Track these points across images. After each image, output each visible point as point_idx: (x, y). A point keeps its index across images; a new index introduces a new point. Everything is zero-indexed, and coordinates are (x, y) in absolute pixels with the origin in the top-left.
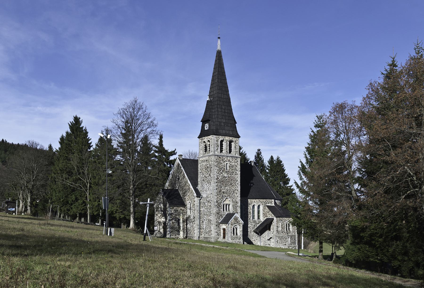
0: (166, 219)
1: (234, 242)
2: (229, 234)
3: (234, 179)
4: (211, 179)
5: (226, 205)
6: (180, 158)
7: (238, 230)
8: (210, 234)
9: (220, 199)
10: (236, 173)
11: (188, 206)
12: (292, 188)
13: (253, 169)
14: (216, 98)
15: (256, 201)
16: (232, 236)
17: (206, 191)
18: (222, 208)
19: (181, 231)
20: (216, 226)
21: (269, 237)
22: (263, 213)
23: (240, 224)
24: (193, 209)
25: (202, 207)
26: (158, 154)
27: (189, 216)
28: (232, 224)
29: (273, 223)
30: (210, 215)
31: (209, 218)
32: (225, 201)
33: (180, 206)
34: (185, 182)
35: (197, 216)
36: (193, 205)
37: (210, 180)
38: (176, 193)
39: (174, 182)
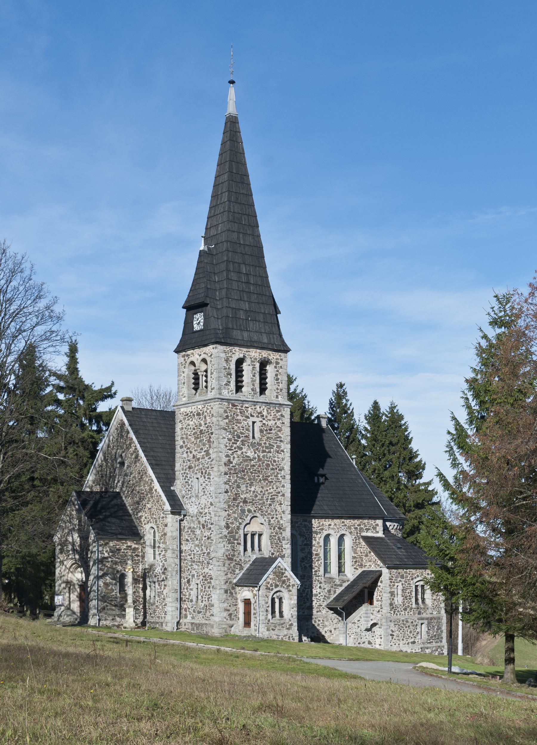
0: (88, 575)
1: (275, 637)
2: (261, 613)
3: (273, 465)
5: (253, 535)
8: (208, 614)
9: (236, 519)
11: (148, 538)
15: (333, 524)
16: (269, 621)
17: (197, 496)
19: (129, 607)
20: (226, 592)
21: (368, 621)
23: (291, 588)
24: (161, 545)
25: (187, 540)
27: (152, 566)
28: (268, 588)
29: (379, 584)
30: (208, 563)
31: (206, 570)
32: (249, 524)
33: (126, 539)
34: (139, 473)
35: (173, 565)
36: (162, 536)
37: (208, 468)
38: (115, 502)
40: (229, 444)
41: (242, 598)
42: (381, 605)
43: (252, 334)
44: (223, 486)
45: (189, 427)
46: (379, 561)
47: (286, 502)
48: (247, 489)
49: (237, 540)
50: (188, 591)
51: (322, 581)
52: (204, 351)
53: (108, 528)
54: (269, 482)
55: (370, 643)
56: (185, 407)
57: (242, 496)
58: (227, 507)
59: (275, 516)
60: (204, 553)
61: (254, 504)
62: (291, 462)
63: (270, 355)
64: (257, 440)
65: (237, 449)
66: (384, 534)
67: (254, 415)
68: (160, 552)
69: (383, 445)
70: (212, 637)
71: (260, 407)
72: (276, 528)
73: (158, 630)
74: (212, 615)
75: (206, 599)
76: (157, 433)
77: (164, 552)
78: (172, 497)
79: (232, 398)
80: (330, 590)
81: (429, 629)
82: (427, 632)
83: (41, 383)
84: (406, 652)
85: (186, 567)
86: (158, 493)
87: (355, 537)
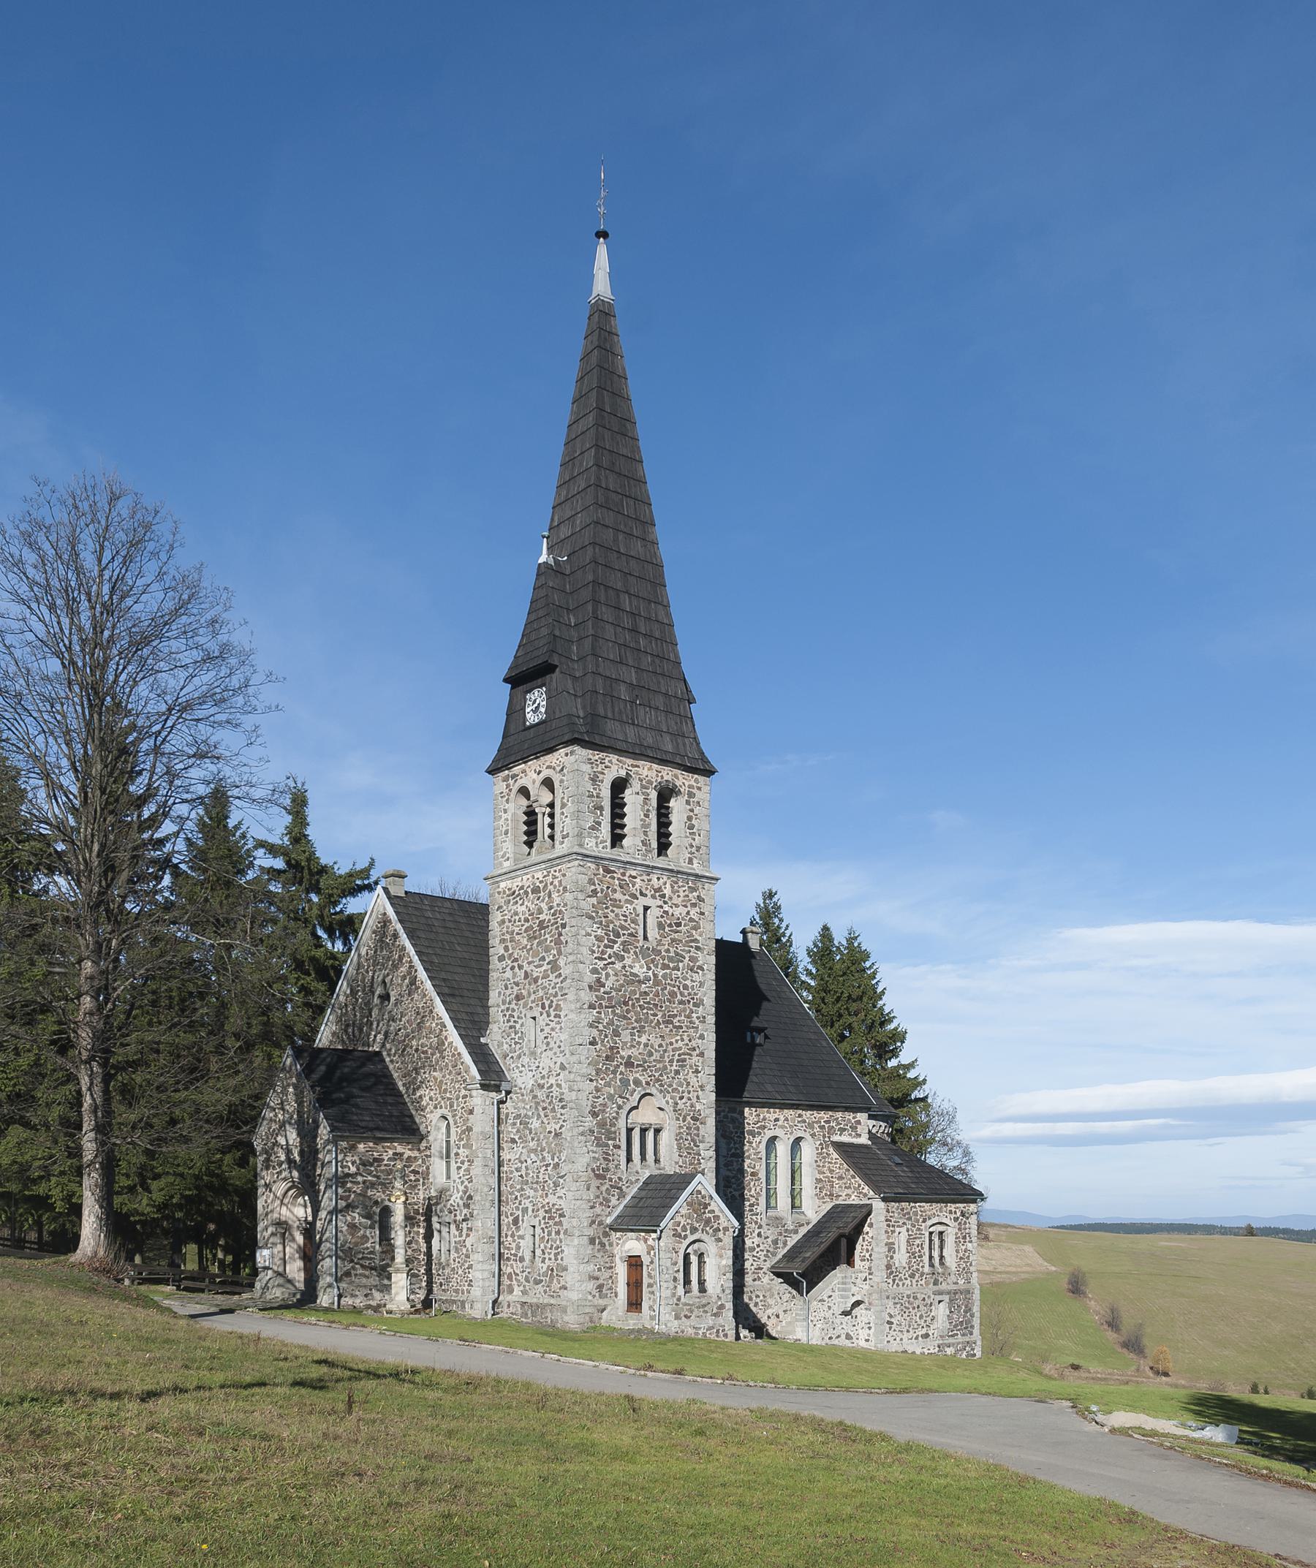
0: (316, 1210)
1: (691, 1331)
3: (682, 994)
4: (561, 988)
5: (644, 1131)
6: (393, 892)
7: (710, 1262)
8: (555, 1285)
9: (611, 1097)
11: (437, 1137)
12: (911, 1075)
13: (757, 966)
14: (590, 550)
15: (782, 1118)
16: (679, 1299)
17: (533, 1054)
18: (619, 1147)
19: (398, 1271)
20: (592, 1241)
22: (819, 1181)
23: (720, 1235)
24: (460, 1151)
25: (513, 1141)
26: (283, 887)
27: (442, 1192)
28: (677, 1235)
29: (866, 1229)
30: (556, 1185)
31: (552, 1199)
33: (392, 1140)
34: (418, 1013)
35: (486, 1189)
36: (463, 1132)
37: (556, 995)
38: (370, 1067)
39: (362, 1017)
40: (599, 947)
41: (624, 1254)
42: (870, 1269)
43: (643, 733)
44: (587, 1031)
45: (517, 918)
46: (867, 1188)
48: (633, 1040)
49: (614, 1139)
50: (514, 1241)
52: (547, 764)
53: (355, 1117)
54: (675, 1027)
56: (508, 879)
57: (623, 1053)
58: (594, 1073)
59: (686, 1095)
60: (547, 1165)
64: (652, 943)
65: (613, 959)
67: (648, 892)
68: (459, 1164)
69: (838, 1000)
70: (565, 1332)
71: (658, 879)
73: (455, 1317)
75: (552, 1256)
76: (453, 939)
77: (466, 1163)
78: (483, 1057)
82: (948, 1316)
83: (239, 861)
84: (914, 1353)
85: (512, 1193)
86: (456, 1049)
87: (821, 1144)
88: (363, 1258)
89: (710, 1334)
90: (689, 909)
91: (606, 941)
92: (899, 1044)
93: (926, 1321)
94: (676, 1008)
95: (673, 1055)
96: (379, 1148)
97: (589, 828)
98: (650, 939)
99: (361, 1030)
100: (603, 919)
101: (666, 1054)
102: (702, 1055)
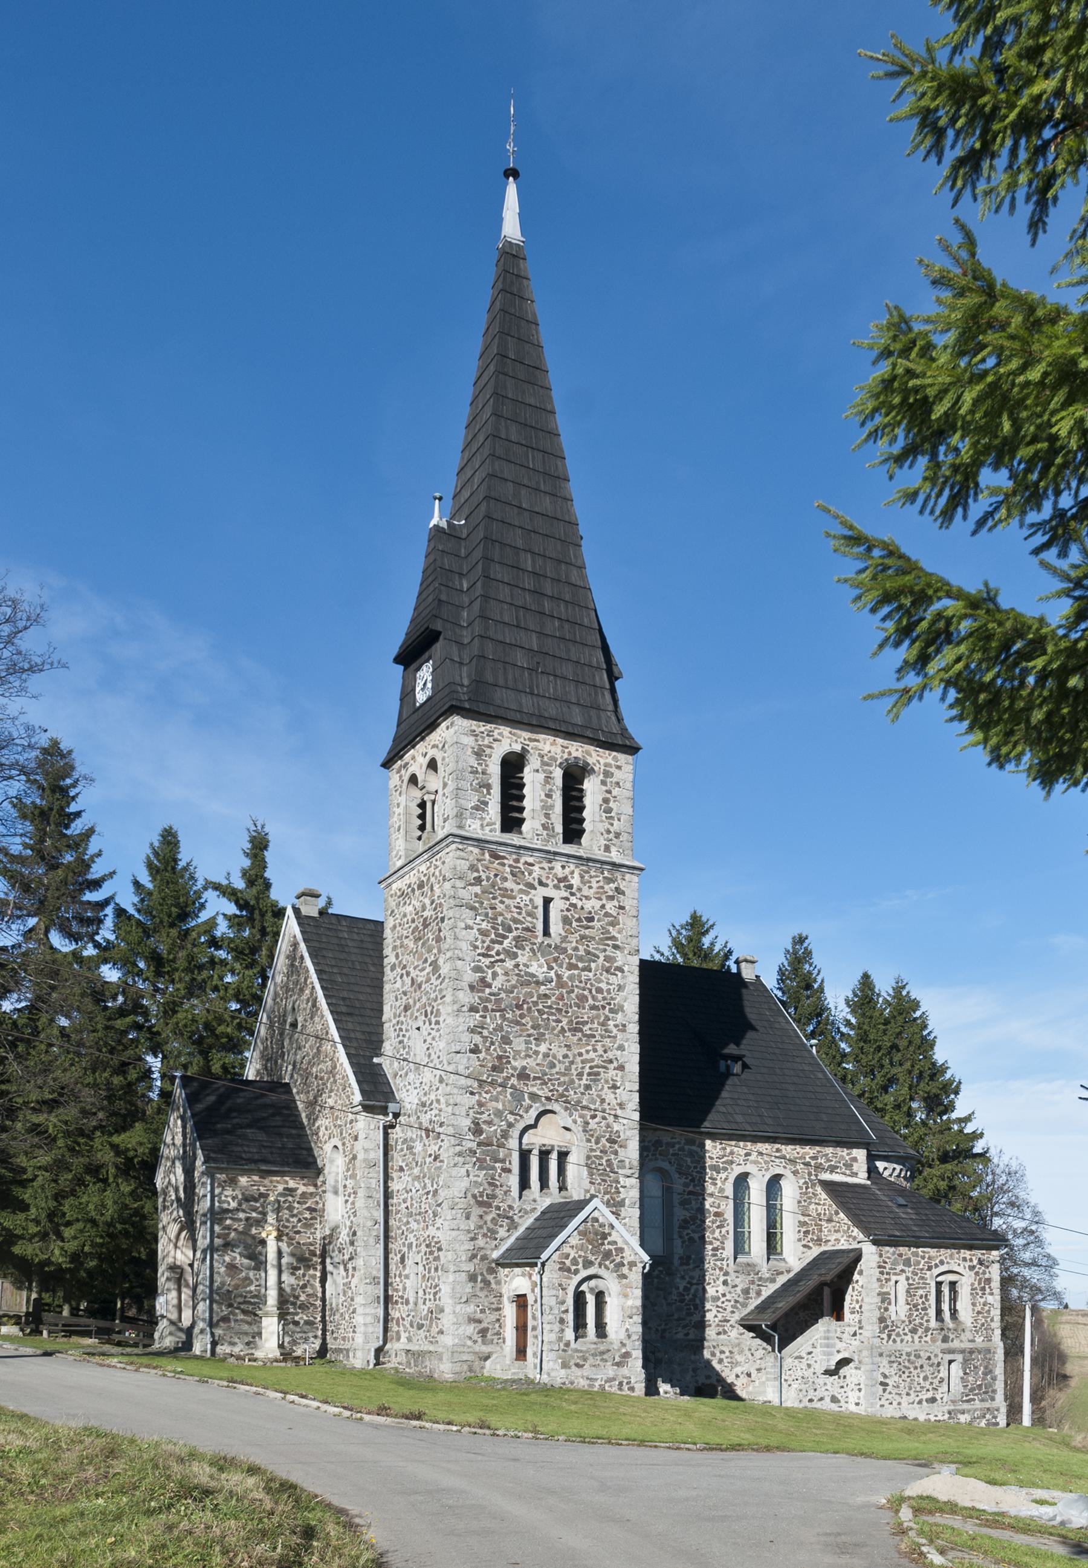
1: (583, 1383)
2: (547, 1327)
3: (594, 998)
5: (544, 1155)
6: (305, 911)
8: (434, 1330)
9: (499, 1114)
10: (608, 959)
12: (969, 1129)
16: (568, 1344)
18: (509, 1171)
19: (267, 1315)
20: (472, 1278)
21: (830, 1354)
23: (625, 1270)
25: (401, 1169)
28: (564, 1268)
29: (856, 1277)
30: (435, 1215)
31: (432, 1231)
32: (534, 1126)
33: (282, 1174)
38: (273, 1097)
40: (484, 942)
41: (512, 1294)
42: (860, 1322)
44: (466, 1037)
46: (856, 1230)
47: (627, 1084)
48: (527, 1049)
49: (503, 1161)
51: (731, 1270)
55: (834, 1400)
60: (428, 1193)
61: (546, 1084)
62: (641, 995)
63: (591, 756)
65: (502, 957)
66: (869, 1178)
67: (549, 882)
71: (563, 867)
72: (603, 1140)
74: (441, 1332)
79: (489, 838)
80: (749, 1289)
81: (965, 1374)
82: (962, 1378)
85: (399, 1228)
87: (806, 1183)
88: (245, 1302)
89: (611, 1386)
90: (604, 901)
91: (493, 936)
92: (952, 1096)
93: (932, 1383)
94: (586, 1014)
95: (583, 1068)
96: (266, 1182)
97: (472, 808)
98: (553, 935)
99: (276, 1062)
100: (490, 911)
101: (574, 1067)
102: (621, 1068)
